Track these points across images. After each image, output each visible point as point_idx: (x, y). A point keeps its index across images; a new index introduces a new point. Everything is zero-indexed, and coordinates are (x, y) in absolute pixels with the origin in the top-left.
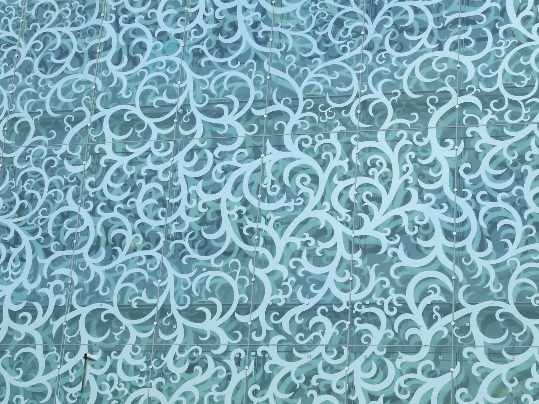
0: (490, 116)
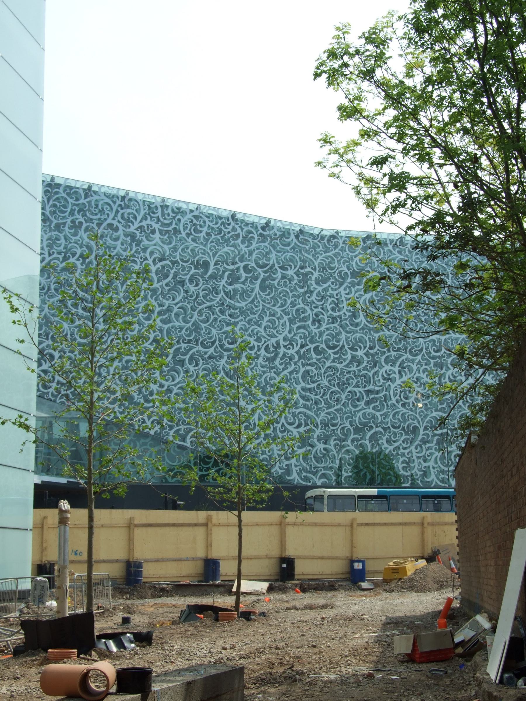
0: (386, 436)
